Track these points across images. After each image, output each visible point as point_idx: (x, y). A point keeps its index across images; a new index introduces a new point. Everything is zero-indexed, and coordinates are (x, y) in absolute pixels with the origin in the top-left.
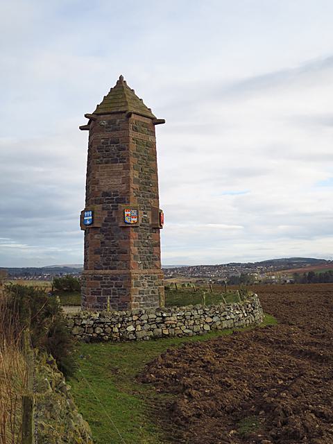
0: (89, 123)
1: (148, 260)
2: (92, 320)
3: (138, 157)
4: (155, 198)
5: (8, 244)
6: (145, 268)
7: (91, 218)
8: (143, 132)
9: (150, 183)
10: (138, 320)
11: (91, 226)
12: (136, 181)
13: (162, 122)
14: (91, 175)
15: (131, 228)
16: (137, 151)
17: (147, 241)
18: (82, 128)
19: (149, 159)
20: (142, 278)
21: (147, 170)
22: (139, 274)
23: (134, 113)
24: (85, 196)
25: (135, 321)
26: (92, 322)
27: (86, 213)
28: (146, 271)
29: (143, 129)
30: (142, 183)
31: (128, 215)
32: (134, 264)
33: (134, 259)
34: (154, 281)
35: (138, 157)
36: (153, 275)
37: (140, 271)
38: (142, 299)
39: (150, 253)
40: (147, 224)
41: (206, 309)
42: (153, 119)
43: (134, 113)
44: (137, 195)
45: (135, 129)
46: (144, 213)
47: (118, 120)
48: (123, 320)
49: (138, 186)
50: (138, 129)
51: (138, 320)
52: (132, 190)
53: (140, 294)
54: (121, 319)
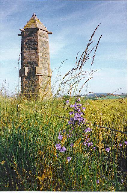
45: (41, 36)
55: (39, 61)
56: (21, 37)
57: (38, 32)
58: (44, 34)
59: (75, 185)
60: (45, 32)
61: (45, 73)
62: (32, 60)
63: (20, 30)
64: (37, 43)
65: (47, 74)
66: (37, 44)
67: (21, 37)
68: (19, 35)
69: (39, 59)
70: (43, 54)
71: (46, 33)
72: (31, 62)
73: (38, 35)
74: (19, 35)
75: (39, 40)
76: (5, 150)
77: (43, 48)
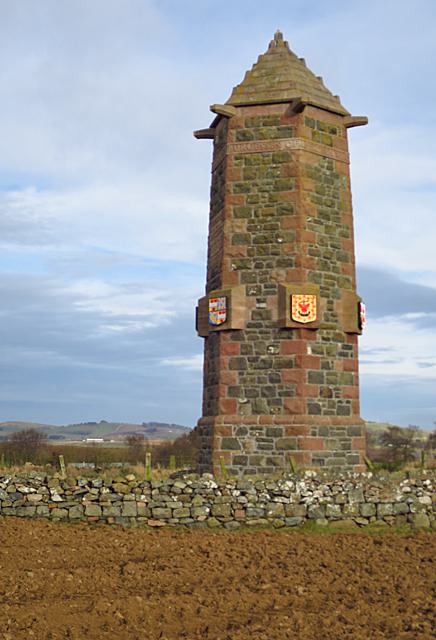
0: (214, 125)
6: (256, 412)
8: (263, 137)
9: (278, 236)
11: (224, 327)
12: (240, 239)
13: (363, 122)
14: (237, 226)
15: (222, 334)
18: (200, 135)
19: (277, 189)
20: (242, 432)
24: (356, 253)
27: (211, 305)
30: (256, 241)
32: (228, 404)
33: (230, 393)
40: (266, 323)
42: (342, 115)
44: (239, 268)
46: (259, 301)
52: (228, 259)
53: (235, 463)
56: (208, 145)
67: (208, 145)
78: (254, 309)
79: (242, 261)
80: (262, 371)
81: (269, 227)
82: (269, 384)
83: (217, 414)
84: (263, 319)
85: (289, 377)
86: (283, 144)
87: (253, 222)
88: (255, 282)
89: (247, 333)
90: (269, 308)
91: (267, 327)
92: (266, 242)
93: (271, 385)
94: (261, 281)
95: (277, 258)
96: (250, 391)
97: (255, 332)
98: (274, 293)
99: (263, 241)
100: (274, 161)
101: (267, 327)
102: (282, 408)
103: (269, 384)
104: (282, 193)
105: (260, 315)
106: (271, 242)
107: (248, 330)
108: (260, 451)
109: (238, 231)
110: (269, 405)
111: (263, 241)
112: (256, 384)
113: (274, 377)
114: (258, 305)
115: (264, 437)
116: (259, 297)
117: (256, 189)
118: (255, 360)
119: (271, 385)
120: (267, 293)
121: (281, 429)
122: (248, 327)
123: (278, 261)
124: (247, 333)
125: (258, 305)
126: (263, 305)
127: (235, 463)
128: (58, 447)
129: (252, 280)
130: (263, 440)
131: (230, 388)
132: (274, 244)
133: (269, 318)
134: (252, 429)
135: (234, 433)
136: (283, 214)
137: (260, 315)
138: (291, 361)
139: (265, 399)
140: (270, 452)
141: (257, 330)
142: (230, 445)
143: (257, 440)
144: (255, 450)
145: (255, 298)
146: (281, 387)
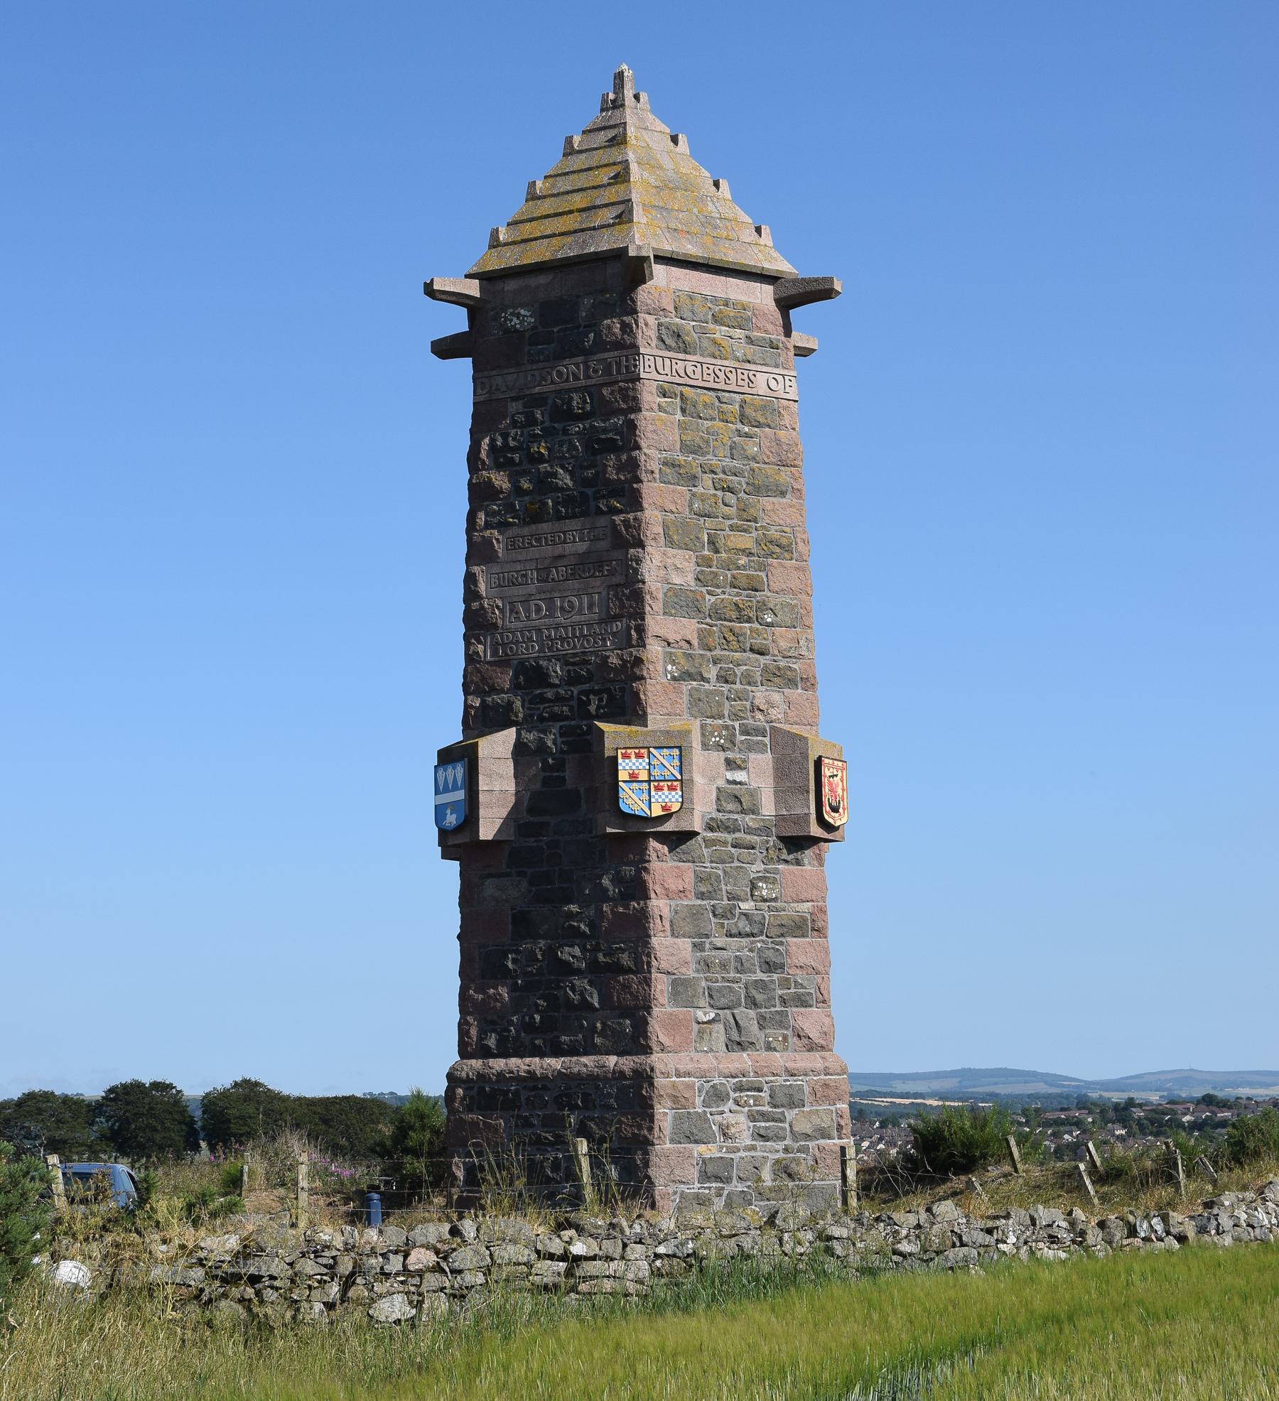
1: (754, 1004)
2: (201, 1263)
3: (693, 479)
4: (792, 683)
5: (974, 1087)
6: (737, 1045)
7: (460, 795)
8: (718, 351)
10: (437, 1269)
12: (681, 603)
16: (686, 448)
17: (746, 906)
20: (717, 1096)
21: (746, 541)
22: (702, 1075)
23: (660, 259)
25: (420, 1274)
26: (199, 1273)
28: (744, 1060)
29: (720, 332)
30: (716, 613)
31: (633, 778)
34: (790, 1114)
35: (693, 479)
36: (780, 1080)
37: (707, 1062)
38: (719, 1204)
39: (769, 966)
40: (749, 820)
41: (837, 1231)
43: (660, 259)
44: (687, 676)
45: (676, 341)
46: (730, 764)
47: (587, 302)
48: (357, 1270)
49: (688, 628)
50: (691, 337)
51: (437, 1269)
53: (705, 1176)
54: (346, 1266)
55: (654, 650)
56: (463, 367)
57: (644, 295)
58: (741, 318)
59: (780, 992)
60: (736, 289)
61: (734, 797)
62: (567, 649)
63: (430, 291)
64: (632, 426)
65: (768, 808)
66: (627, 439)
67: (463, 367)
68: (446, 349)
69: (658, 623)
70: (704, 562)
71: (763, 296)
72: (557, 670)
73: (647, 331)
74: (446, 349)
75: (649, 395)
76: (381, 1144)
77: (705, 485)
78: (721, 783)
79: (689, 657)
80: (745, 941)
81: (743, 582)
82: (760, 975)
83: (652, 1053)
84: (743, 812)
85: (802, 960)
86: (761, 380)
87: (707, 562)
88: (721, 716)
89: (709, 843)
90: (754, 785)
91: (749, 831)
92: (739, 620)
93: (764, 977)
94: (735, 716)
95: (763, 660)
96: (719, 990)
97: (725, 843)
98: (760, 748)
99: (734, 615)
100: (743, 418)
101: (749, 831)
102: (789, 1033)
103: (760, 975)
104: (767, 502)
105: (737, 799)
106: (749, 620)
107: (710, 834)
108: (759, 1144)
109: (677, 580)
110: (761, 1027)
111: (734, 615)
112: (732, 975)
113: (770, 955)
114: (730, 776)
115: (767, 1108)
116: (730, 755)
117: (707, 479)
118: (728, 913)
119: (764, 977)
120: (750, 748)
121: (800, 1088)
122: (711, 829)
123: (765, 670)
124: (709, 843)
125: (730, 776)
126: (740, 776)
127: (705, 1176)
128: (1008, 1096)
129: (715, 711)
130: (764, 1116)
131: (674, 983)
132: (756, 625)
133: (754, 811)
134: (740, 1088)
135: (698, 1101)
136: (771, 554)
137: (737, 799)
138: (804, 920)
139: (752, 1013)
140: (780, 1146)
141: (729, 837)
142: (691, 1133)
143: (752, 1117)
144: (749, 1142)
145: (722, 755)
146: (785, 983)
